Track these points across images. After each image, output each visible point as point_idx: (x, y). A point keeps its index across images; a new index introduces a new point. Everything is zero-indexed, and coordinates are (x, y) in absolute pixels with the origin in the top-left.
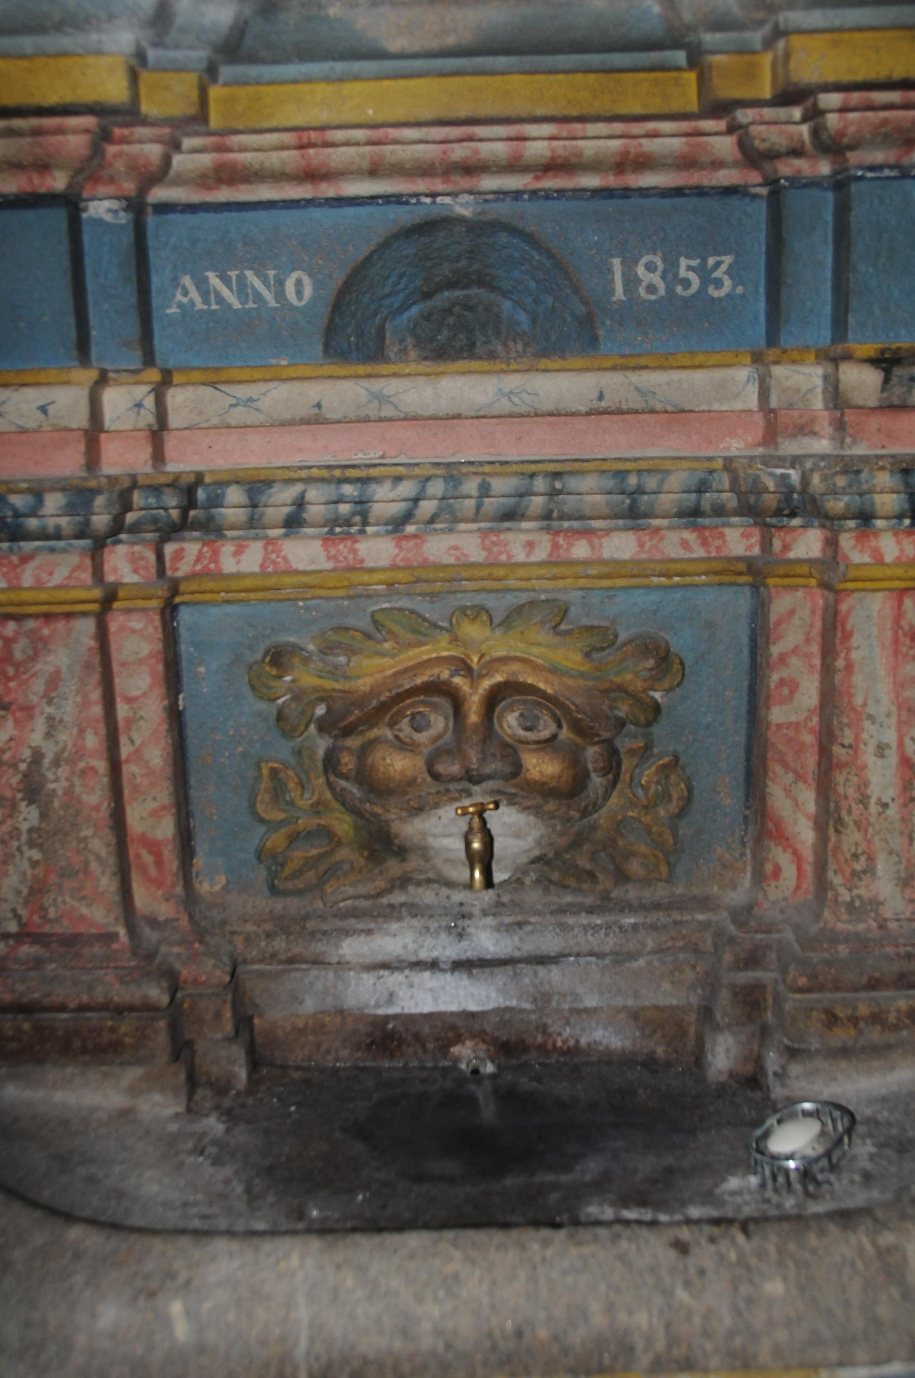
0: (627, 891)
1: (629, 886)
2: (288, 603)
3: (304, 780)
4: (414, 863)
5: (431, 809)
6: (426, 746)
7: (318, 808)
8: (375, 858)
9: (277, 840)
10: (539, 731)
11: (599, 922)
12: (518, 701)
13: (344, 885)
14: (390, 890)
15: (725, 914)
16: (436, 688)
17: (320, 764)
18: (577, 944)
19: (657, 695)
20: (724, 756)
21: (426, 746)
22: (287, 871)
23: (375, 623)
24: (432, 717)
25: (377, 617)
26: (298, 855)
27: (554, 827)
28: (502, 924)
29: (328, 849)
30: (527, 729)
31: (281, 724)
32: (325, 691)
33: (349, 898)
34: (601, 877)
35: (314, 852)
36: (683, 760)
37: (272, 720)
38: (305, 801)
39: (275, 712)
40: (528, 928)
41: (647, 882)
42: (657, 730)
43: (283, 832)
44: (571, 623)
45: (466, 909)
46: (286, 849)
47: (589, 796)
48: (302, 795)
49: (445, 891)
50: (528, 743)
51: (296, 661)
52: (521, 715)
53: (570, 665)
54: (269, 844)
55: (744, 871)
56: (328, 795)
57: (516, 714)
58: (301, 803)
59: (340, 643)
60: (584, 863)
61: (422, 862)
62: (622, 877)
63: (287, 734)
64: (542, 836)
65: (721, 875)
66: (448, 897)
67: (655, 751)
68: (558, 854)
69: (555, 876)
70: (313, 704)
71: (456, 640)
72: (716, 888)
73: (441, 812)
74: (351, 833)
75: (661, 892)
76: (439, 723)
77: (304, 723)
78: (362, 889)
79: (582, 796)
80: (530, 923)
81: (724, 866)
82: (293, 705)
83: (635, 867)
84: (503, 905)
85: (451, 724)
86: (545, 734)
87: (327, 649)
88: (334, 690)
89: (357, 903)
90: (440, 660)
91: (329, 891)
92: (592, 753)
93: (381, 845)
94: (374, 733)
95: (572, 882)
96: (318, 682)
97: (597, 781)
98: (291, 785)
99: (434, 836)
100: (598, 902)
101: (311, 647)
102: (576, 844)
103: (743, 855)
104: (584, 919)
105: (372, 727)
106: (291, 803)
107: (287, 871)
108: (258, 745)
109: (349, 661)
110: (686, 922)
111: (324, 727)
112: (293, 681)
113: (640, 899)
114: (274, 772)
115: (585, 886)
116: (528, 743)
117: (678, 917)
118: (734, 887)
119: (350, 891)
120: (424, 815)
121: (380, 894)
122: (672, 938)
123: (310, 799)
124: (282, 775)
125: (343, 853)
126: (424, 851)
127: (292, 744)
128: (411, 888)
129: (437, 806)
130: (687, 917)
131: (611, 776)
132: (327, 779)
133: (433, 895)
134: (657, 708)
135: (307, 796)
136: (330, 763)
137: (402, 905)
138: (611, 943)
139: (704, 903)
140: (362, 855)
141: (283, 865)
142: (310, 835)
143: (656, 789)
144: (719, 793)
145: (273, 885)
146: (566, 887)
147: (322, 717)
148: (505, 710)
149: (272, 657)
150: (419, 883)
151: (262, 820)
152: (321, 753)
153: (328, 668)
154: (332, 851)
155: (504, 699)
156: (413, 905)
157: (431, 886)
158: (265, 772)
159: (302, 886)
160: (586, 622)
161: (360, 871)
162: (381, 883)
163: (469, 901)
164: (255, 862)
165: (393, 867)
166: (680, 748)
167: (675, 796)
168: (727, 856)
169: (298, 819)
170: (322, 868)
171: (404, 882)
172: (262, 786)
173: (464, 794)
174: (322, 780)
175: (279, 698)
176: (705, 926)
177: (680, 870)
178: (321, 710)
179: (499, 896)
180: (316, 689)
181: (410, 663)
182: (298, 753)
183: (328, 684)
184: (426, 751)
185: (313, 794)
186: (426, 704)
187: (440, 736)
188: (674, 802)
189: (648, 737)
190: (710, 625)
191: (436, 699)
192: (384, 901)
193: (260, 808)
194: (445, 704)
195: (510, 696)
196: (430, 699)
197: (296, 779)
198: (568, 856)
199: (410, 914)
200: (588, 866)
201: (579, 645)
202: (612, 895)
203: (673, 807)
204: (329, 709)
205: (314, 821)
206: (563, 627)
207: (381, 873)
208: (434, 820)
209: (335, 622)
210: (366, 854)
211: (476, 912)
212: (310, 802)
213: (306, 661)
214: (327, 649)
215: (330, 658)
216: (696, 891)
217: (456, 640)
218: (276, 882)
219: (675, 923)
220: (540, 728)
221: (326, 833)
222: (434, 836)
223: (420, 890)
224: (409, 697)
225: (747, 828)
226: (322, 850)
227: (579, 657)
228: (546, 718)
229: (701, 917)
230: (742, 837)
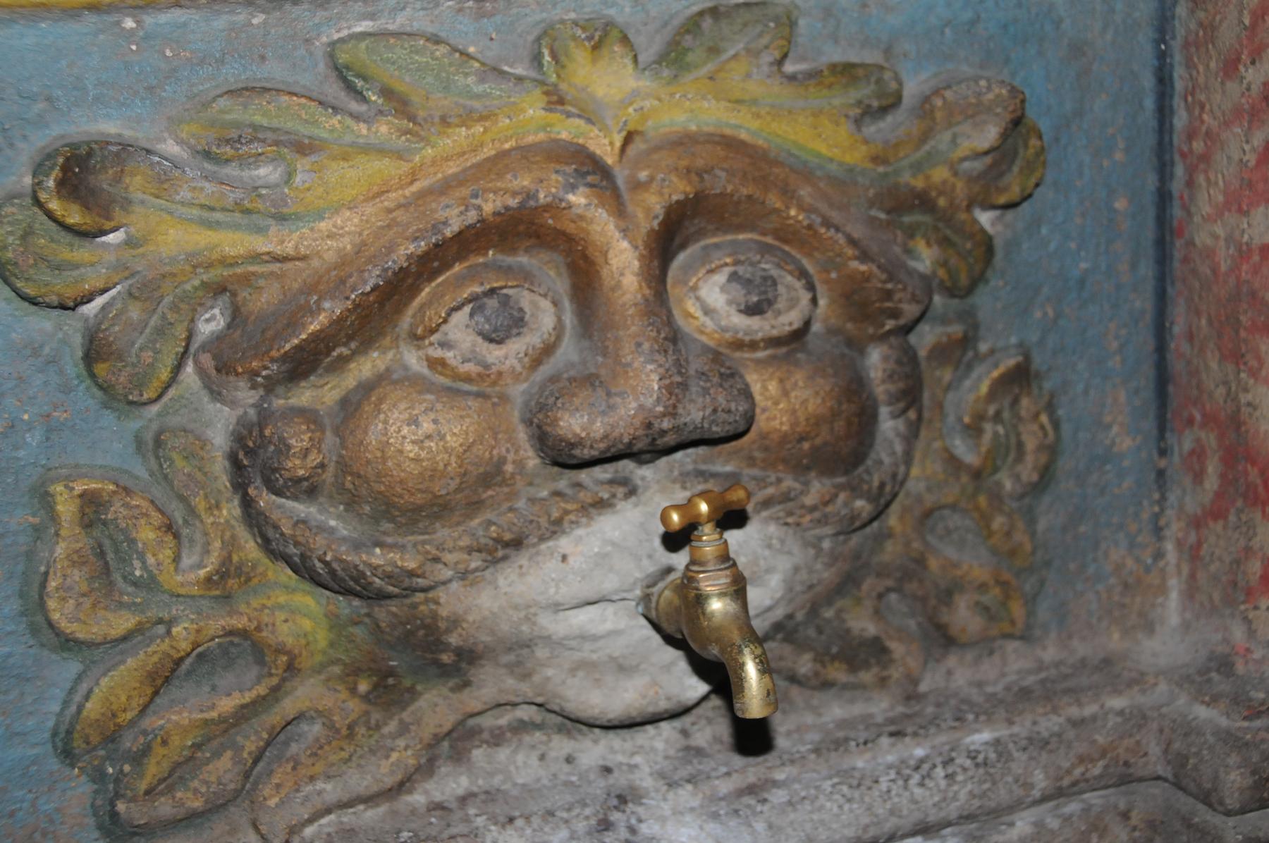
0: (949, 673)
1: (952, 661)
2: (91, 19)
3: (178, 517)
4: (491, 683)
5: (542, 539)
6: (517, 377)
7: (226, 581)
8: (388, 692)
9: (115, 686)
10: (779, 313)
11: (919, 752)
12: (717, 246)
13: (312, 779)
14: (426, 769)
15: (1163, 687)
16: (523, 228)
17: (219, 468)
18: (892, 812)
19: (985, 218)
20: (1115, 345)
21: (517, 377)
22: (154, 769)
23: (342, 73)
24: (525, 299)
25: (343, 58)
26: (181, 714)
27: (816, 545)
28: (714, 799)
29: (262, 690)
30: (752, 310)
31: (101, 369)
32: (224, 262)
33: (328, 811)
34: (897, 648)
35: (227, 705)
36: (1038, 362)
37: (72, 364)
38: (196, 567)
39: (77, 340)
40: (778, 796)
41: (986, 645)
42: (985, 301)
43: (133, 665)
44: (803, 59)
45: (620, 780)
46: (144, 710)
47: (880, 462)
48: (177, 559)
49: (561, 746)
50: (753, 345)
51: (136, 184)
52: (734, 277)
53: (824, 150)
54: (93, 708)
55: (1163, 590)
56: (250, 549)
57: (721, 278)
58: (172, 579)
59: (256, 127)
60: (863, 624)
61: (510, 682)
62: (942, 639)
63: (118, 399)
64: (796, 569)
65: (1123, 606)
66: (569, 760)
67: (983, 347)
68: (814, 611)
69: (805, 664)
70: (193, 306)
71: (561, 101)
72: (1116, 636)
73: (564, 543)
74: (322, 638)
75: (1015, 664)
76: (545, 313)
77: (169, 361)
78: (359, 781)
79: (869, 462)
80: (775, 784)
81: (1126, 586)
82: (135, 312)
83: (963, 616)
84: (699, 752)
85: (569, 319)
86: (789, 320)
87: (223, 147)
88: (256, 257)
89: (347, 817)
90: (526, 155)
91: (272, 802)
92: (876, 360)
93: (411, 654)
94: (366, 367)
95: (838, 673)
96: (202, 239)
97: (889, 425)
98: (146, 534)
99: (557, 607)
100: (900, 709)
101: (171, 147)
102: (846, 584)
103: (1159, 555)
104: (889, 753)
105: (367, 345)
106: (149, 584)
107: (154, 769)
108: (33, 439)
109: (289, 176)
110: (1094, 718)
111: (224, 363)
112: (130, 243)
113: (980, 685)
114: (92, 507)
115: (866, 676)
116: (753, 345)
117: (1074, 712)
118: (1150, 628)
119: (330, 790)
120: (522, 559)
121: (402, 787)
122: (1081, 759)
123: (200, 566)
124: (117, 511)
125: (306, 694)
126: (519, 650)
127: (134, 425)
128: (478, 754)
129: (557, 527)
130: (1090, 710)
131: (912, 414)
132: (247, 503)
133: (534, 760)
134: (987, 245)
135: (186, 561)
136: (253, 461)
137: (464, 800)
138: (963, 795)
139: (1109, 671)
140: (353, 691)
141: (139, 758)
142: (205, 661)
143: (996, 434)
144: (1108, 427)
145: (114, 815)
146: (826, 685)
147: (219, 338)
148: (688, 269)
149: (65, 168)
150: (497, 739)
151: (68, 644)
152: (219, 439)
153: (232, 196)
154: (276, 692)
155: (683, 246)
156: (490, 796)
157: (527, 739)
158: (66, 508)
159: (197, 804)
160: (836, 54)
161: (351, 736)
162: (404, 755)
163: (620, 758)
164: (54, 764)
165: (435, 707)
166: (1034, 337)
167: (1030, 444)
168: (1130, 563)
169: (170, 623)
170: (250, 746)
171: (459, 740)
172: (60, 550)
173: (621, 491)
174: (231, 510)
175: (88, 299)
176: (1137, 719)
177: (1044, 612)
178: (211, 323)
179: (685, 733)
180: (197, 262)
181: (452, 169)
182: (155, 446)
183: (234, 242)
184: (518, 391)
185: (206, 551)
186: (508, 271)
187: (548, 350)
188: (1029, 459)
189: (970, 319)
190: (1077, 50)
191: (523, 259)
192: (417, 798)
193: (59, 612)
194: (551, 272)
195: (701, 234)
196: (509, 260)
197: (156, 518)
198: (829, 613)
199: (494, 819)
200: (871, 629)
201: (837, 102)
202: (923, 687)
203: (1028, 472)
204: (236, 316)
205: (218, 623)
206: (789, 68)
207: (404, 729)
208: (551, 567)
209: (233, 74)
210: (363, 687)
211: (645, 780)
212: (202, 573)
213: (164, 182)
214: (223, 147)
215: (231, 171)
216: (1081, 649)
217: (561, 101)
218: (121, 807)
219: (1076, 723)
220: (781, 304)
221: (248, 646)
222: (557, 607)
223: (502, 754)
224: (460, 257)
225: (1163, 498)
226: (248, 697)
227: (844, 131)
228: (789, 278)
229: (1117, 703)
230: (1157, 517)
